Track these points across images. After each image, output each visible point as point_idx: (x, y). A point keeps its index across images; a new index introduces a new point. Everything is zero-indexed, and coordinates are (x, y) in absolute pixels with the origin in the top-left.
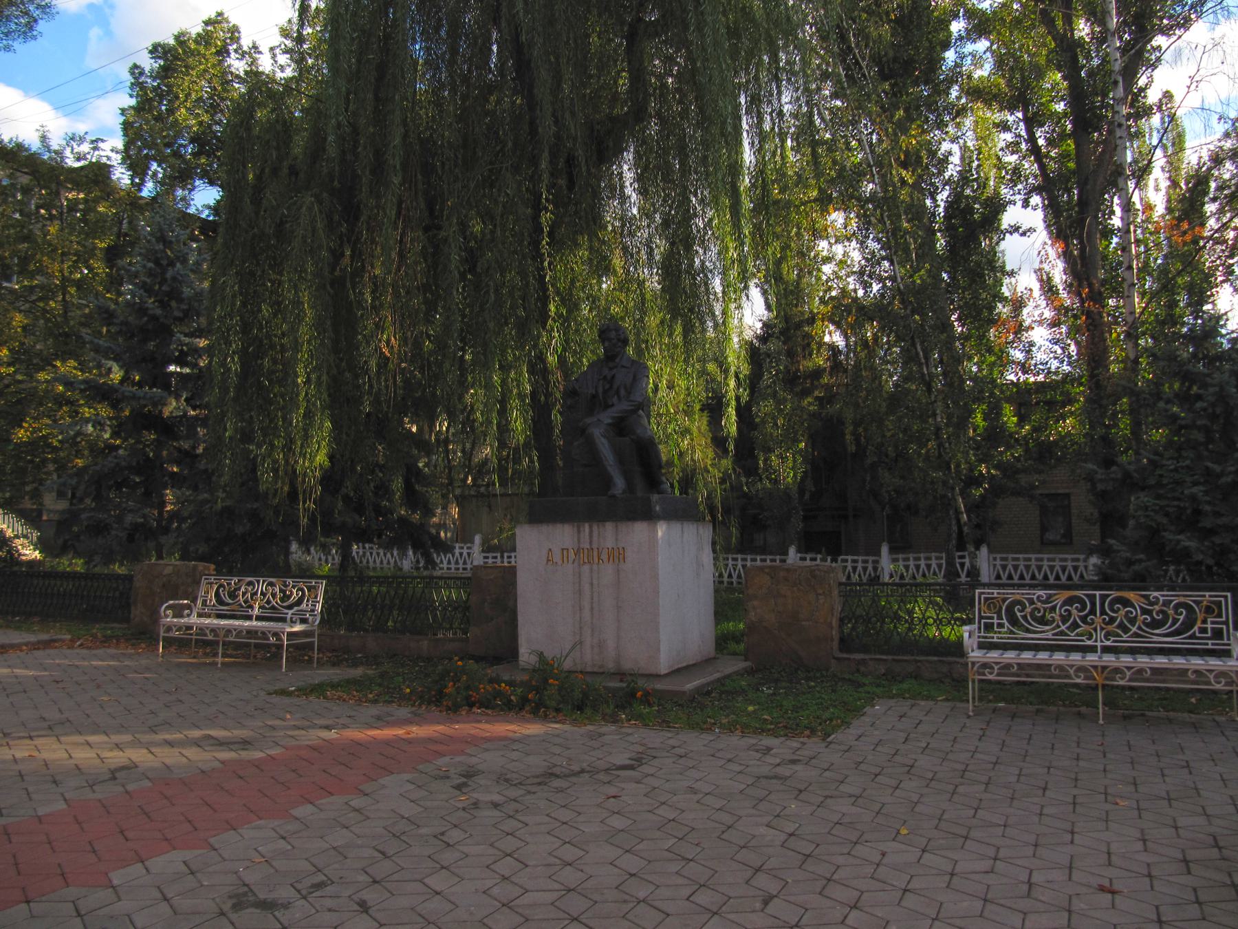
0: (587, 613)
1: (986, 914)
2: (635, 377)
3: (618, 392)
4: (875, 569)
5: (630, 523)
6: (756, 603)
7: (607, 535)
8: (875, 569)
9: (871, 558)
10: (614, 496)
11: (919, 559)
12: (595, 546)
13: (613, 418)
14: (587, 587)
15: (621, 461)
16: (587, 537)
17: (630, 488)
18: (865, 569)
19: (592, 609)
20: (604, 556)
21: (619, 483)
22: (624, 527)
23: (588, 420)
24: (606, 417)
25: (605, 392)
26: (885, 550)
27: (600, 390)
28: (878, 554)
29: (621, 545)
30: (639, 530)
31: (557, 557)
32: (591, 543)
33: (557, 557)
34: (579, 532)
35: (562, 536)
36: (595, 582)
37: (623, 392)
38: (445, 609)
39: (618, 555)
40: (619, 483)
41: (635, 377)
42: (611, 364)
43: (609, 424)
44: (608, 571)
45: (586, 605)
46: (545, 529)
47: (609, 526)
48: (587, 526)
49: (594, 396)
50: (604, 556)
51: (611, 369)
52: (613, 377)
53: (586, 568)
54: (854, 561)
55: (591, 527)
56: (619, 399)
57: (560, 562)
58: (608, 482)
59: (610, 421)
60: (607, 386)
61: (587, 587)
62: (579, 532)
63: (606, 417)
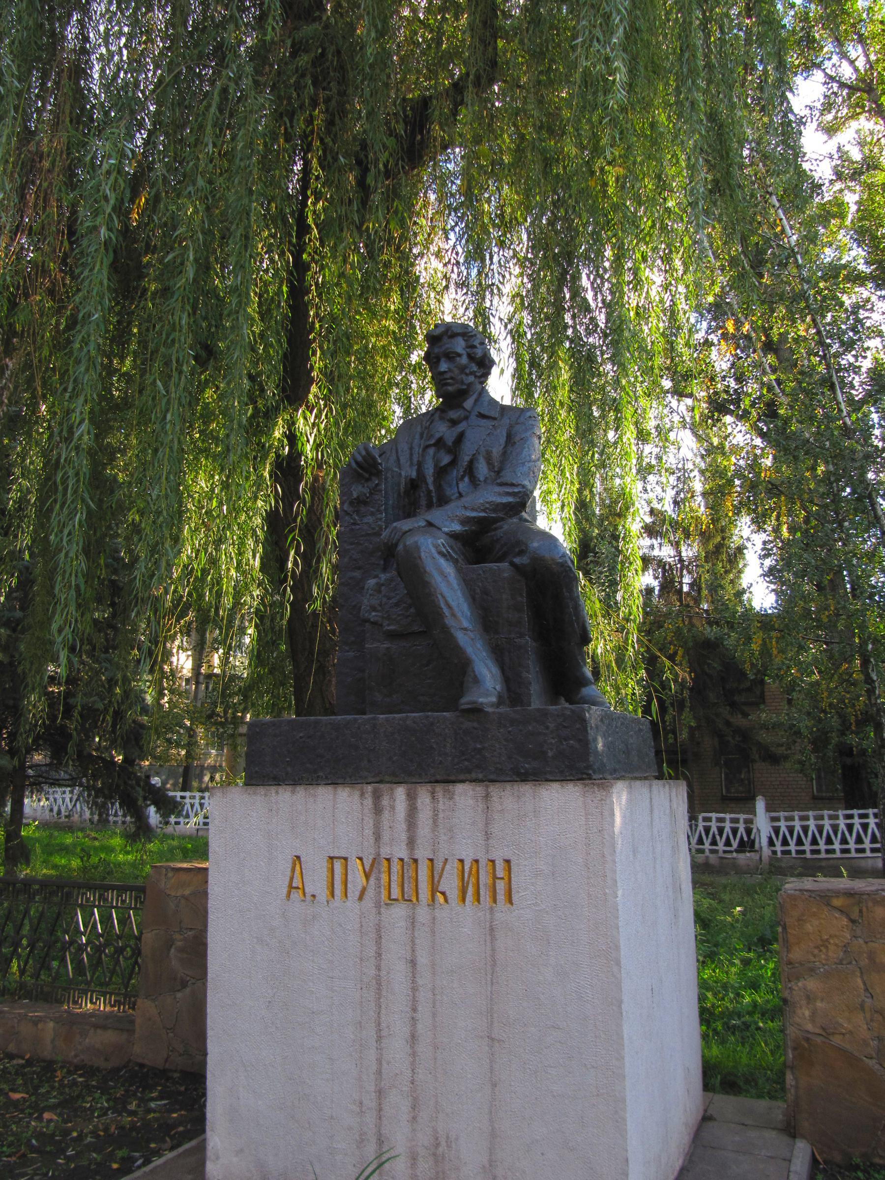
0: (397, 1048)
1: (497, 881)
2: (510, 439)
3: (470, 470)
4: (749, 831)
5: (526, 789)
6: (811, 984)
7: (460, 819)
8: (749, 831)
9: (742, 817)
10: (476, 711)
11: (806, 818)
12: (423, 854)
13: (465, 521)
14: (398, 973)
15: (488, 621)
16: (401, 826)
17: (513, 692)
18: (735, 831)
19: (413, 1038)
20: (450, 883)
21: (488, 680)
22: (511, 799)
23: (405, 525)
24: (450, 520)
25: (441, 472)
26: (760, 805)
27: (429, 471)
28: (753, 812)
29: (498, 856)
30: (557, 804)
31: (317, 884)
32: (411, 843)
33: (317, 884)
34: (378, 810)
35: (330, 819)
36: (423, 959)
37: (482, 470)
38: (99, 950)
39: (489, 883)
40: (488, 680)
41: (510, 439)
42: (453, 414)
43: (454, 536)
44: (462, 921)
45: (399, 1028)
46: (286, 800)
47: (466, 796)
48: (400, 792)
49: (414, 485)
50: (450, 883)
51: (454, 423)
52: (460, 438)
53: (399, 911)
54: (735, 821)
55: (411, 797)
56: (474, 482)
57: (322, 893)
58: (459, 672)
59: (457, 527)
60: (446, 459)
61: (398, 973)
62: (378, 810)
63: (450, 520)
